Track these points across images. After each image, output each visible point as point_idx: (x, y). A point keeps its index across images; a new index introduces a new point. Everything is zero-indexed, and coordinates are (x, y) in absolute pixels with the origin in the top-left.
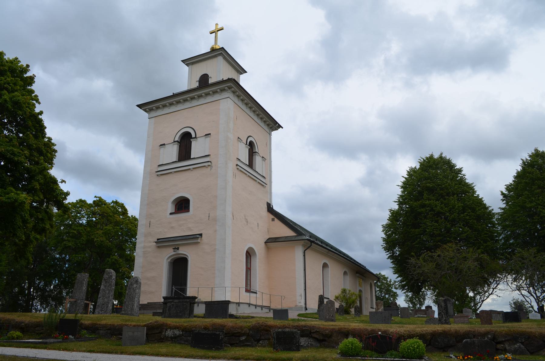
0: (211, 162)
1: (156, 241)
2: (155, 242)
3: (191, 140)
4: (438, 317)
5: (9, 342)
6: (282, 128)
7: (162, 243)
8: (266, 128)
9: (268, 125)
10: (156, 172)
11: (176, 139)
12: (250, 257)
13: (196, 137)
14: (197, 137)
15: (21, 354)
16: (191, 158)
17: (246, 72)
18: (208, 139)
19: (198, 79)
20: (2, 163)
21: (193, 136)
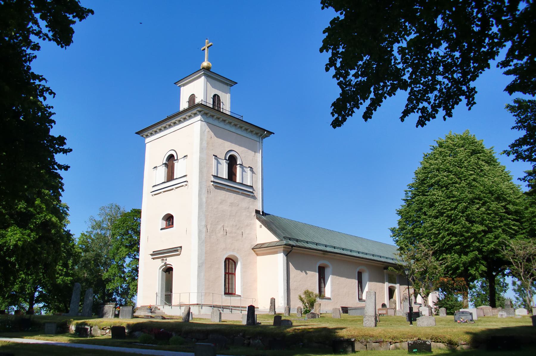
0: (187, 181)
1: (152, 253)
2: (151, 255)
3: (174, 162)
4: (414, 312)
5: (482, 325)
6: (274, 134)
7: (156, 254)
8: (255, 138)
9: (257, 134)
10: (151, 192)
11: (164, 162)
12: (234, 264)
13: (177, 159)
14: (178, 159)
15: (150, 354)
16: (175, 178)
17: (237, 83)
18: (186, 160)
19: (188, 100)
20: (427, 1)
21: (176, 158)
